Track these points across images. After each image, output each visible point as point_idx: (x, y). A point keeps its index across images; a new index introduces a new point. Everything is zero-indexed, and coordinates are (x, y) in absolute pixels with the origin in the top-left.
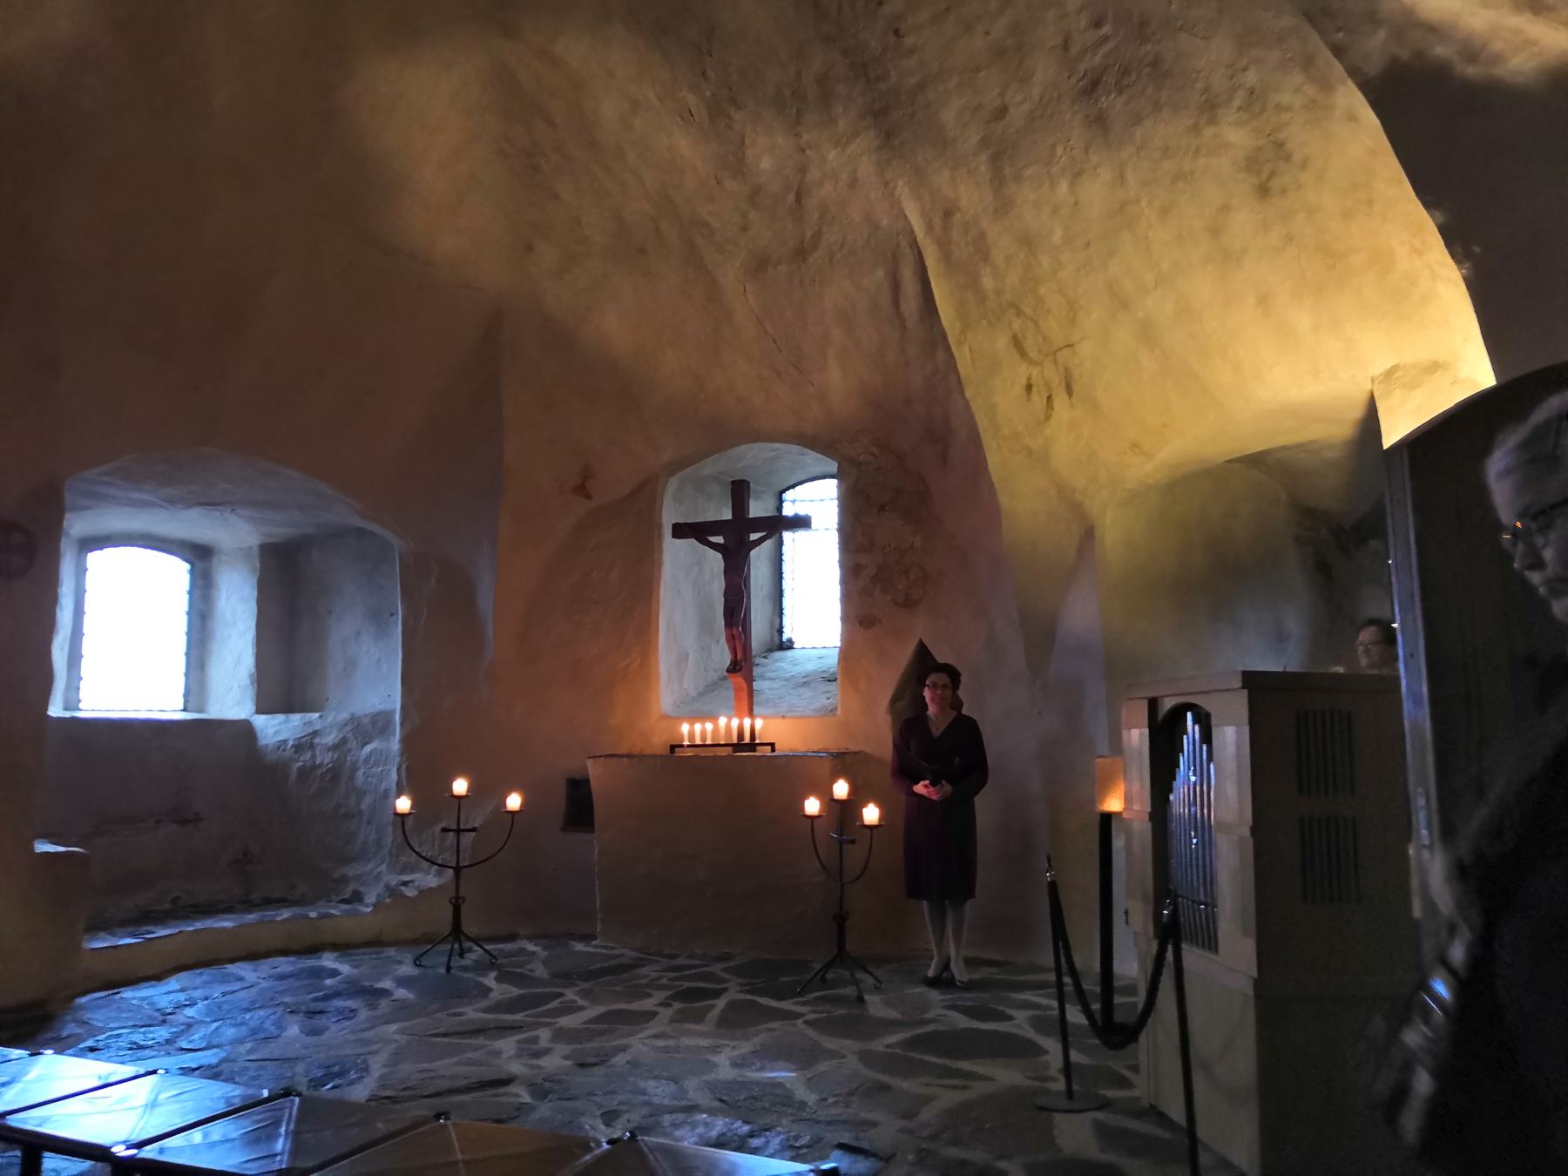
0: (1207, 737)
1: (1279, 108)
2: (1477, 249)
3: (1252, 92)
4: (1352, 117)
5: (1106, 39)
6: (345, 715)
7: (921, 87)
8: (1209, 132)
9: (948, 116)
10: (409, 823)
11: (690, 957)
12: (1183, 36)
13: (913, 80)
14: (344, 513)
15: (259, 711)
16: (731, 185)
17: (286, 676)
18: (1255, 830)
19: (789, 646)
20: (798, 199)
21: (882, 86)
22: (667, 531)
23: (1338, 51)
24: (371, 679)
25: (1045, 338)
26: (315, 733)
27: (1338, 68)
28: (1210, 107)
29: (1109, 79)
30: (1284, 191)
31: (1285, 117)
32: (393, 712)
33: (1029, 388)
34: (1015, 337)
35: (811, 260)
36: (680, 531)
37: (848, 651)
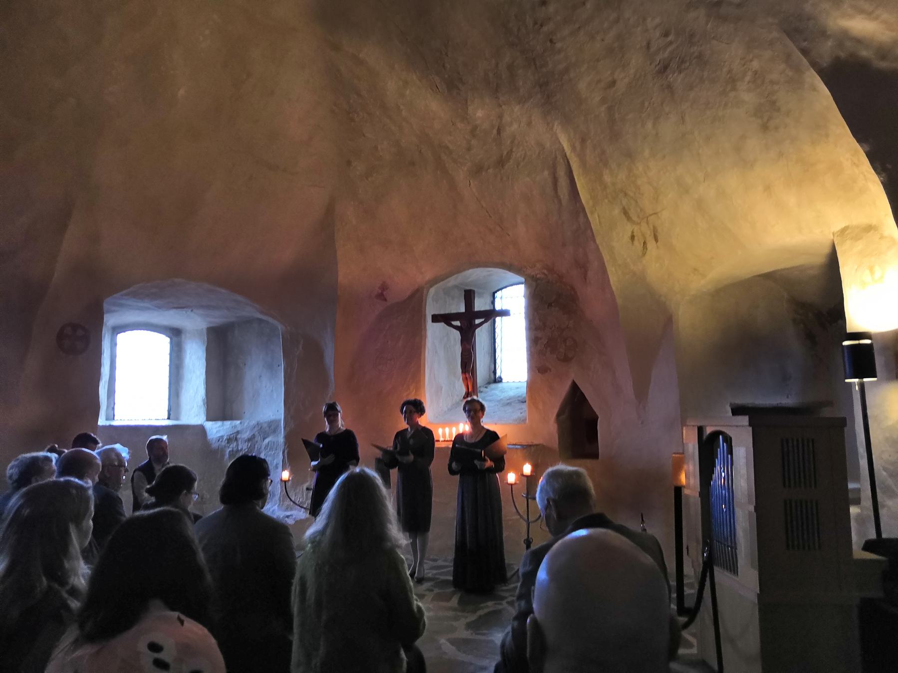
0: (730, 451)
1: (772, 82)
2: (889, 166)
3: (756, 73)
4: (814, 89)
5: (671, 43)
6: (254, 422)
7: (567, 70)
8: (732, 94)
9: (582, 86)
10: (289, 484)
11: (445, 561)
12: (714, 42)
13: (561, 67)
14: (250, 311)
15: (208, 419)
16: (460, 125)
17: (221, 405)
18: (756, 509)
19: (500, 380)
20: (499, 132)
21: (544, 70)
22: (429, 319)
23: (805, 52)
24: (267, 402)
25: (641, 210)
26: (238, 432)
27: (805, 61)
28: (732, 81)
29: (673, 65)
30: (777, 128)
31: (776, 87)
32: (280, 420)
33: (633, 237)
34: (624, 208)
35: (506, 167)
36: (436, 318)
37: (531, 385)
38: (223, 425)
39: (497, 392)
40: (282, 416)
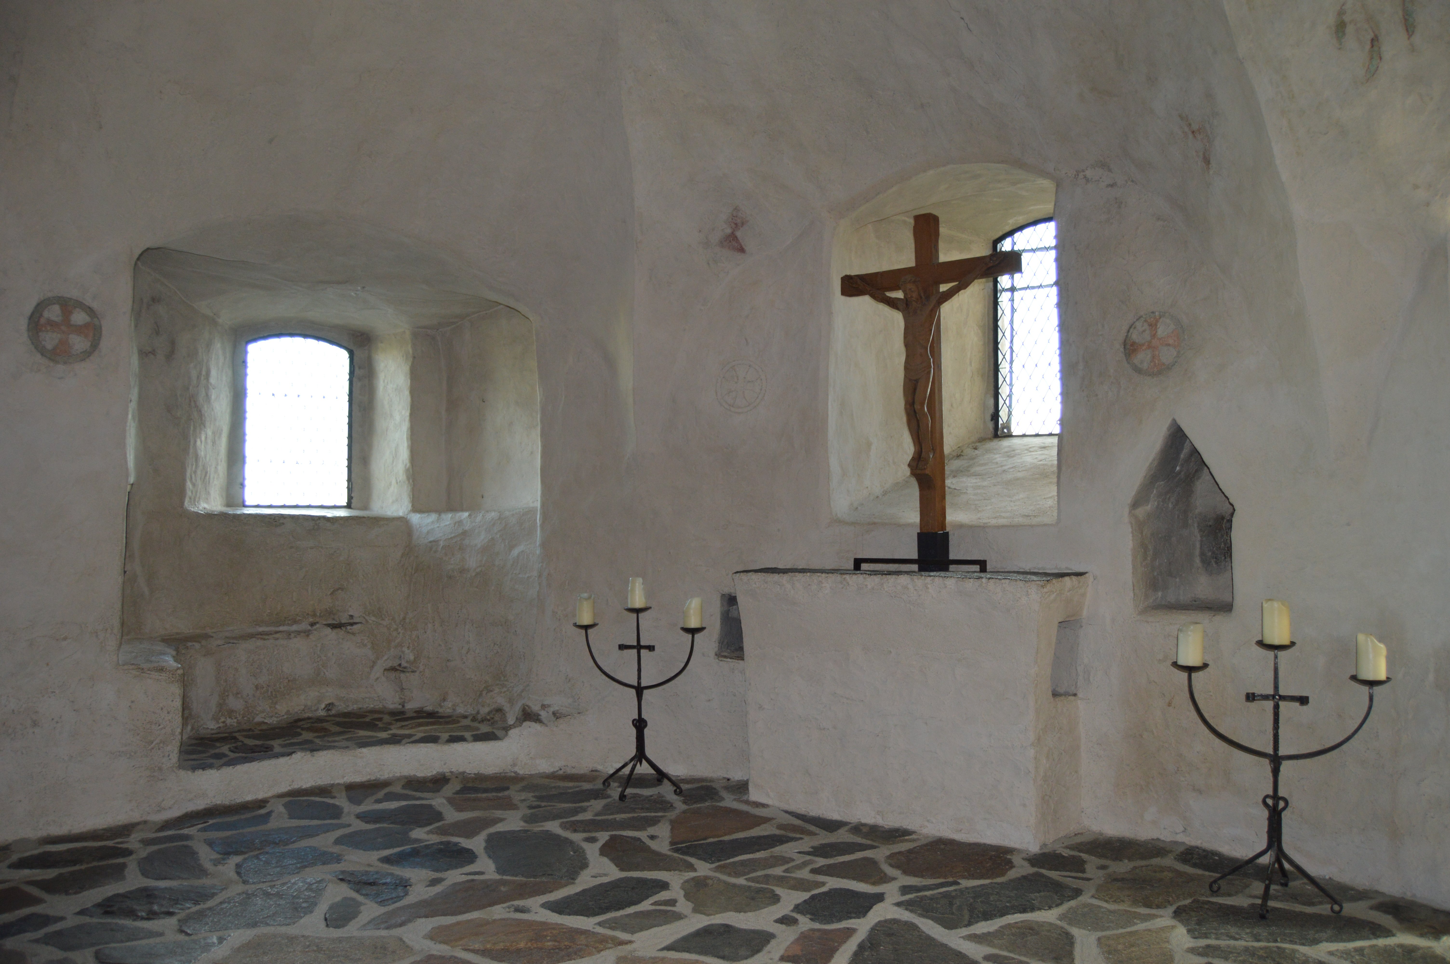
15: (415, 509)
17: (447, 467)
26: (465, 533)
36: (853, 286)
38: (438, 520)
39: (998, 458)
40: (538, 505)
